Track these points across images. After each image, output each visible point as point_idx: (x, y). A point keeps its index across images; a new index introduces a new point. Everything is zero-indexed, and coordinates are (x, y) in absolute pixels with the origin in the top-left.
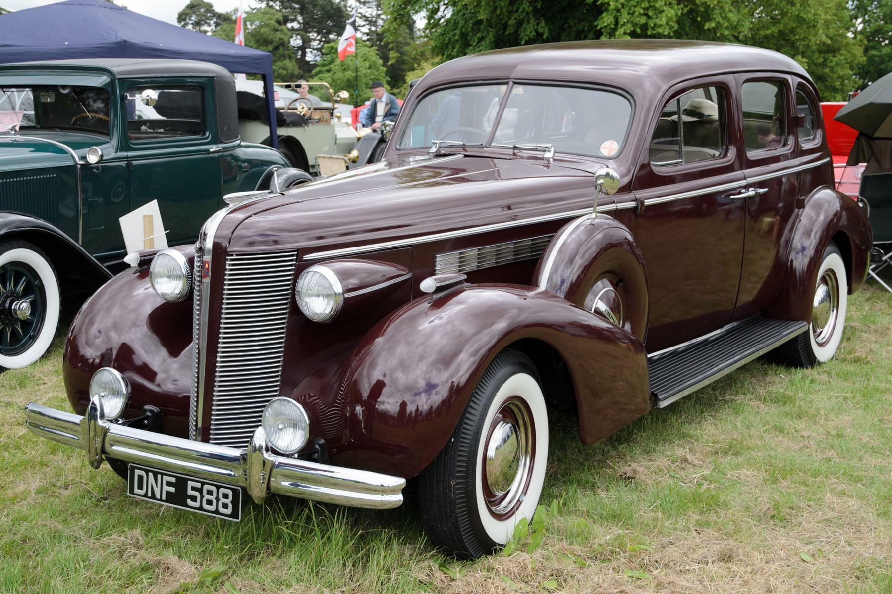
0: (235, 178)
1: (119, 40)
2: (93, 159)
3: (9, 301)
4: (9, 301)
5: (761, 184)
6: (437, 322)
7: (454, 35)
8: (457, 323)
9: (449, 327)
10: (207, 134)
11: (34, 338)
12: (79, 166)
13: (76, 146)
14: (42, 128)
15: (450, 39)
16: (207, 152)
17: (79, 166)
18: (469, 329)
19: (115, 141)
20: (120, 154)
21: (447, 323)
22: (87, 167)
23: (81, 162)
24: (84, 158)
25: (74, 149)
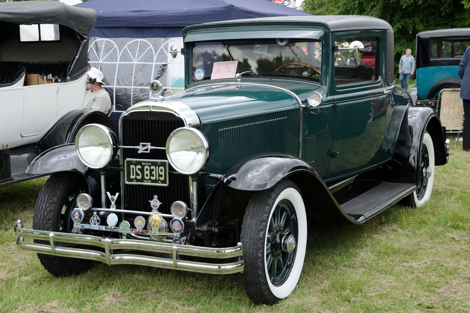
0: (384, 113)
1: (227, 5)
2: (314, 103)
3: (278, 236)
4: (278, 236)
5: (390, 90)
6: (256, 174)
7: (355, 4)
8: (265, 174)
9: (262, 176)
10: (380, 78)
11: (290, 267)
12: (301, 109)
13: (298, 92)
14: (264, 75)
15: (351, 7)
16: (382, 93)
17: (301, 109)
18: (267, 176)
19: (325, 88)
20: (330, 98)
21: (261, 174)
22: (308, 109)
23: (304, 106)
24: (305, 102)
25: (297, 94)
